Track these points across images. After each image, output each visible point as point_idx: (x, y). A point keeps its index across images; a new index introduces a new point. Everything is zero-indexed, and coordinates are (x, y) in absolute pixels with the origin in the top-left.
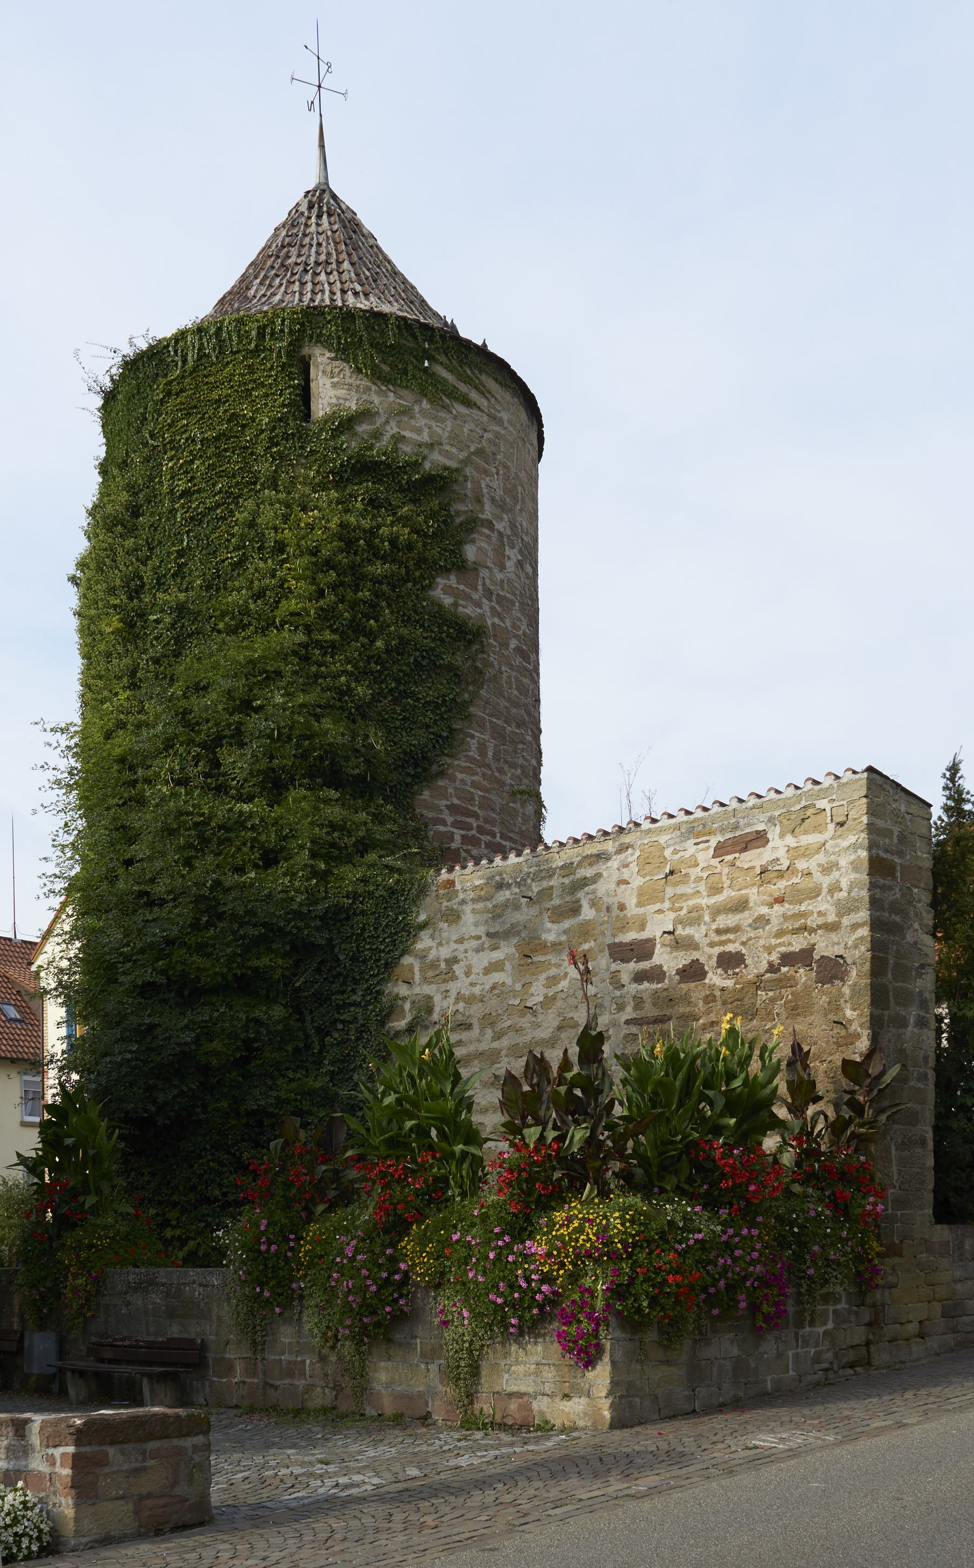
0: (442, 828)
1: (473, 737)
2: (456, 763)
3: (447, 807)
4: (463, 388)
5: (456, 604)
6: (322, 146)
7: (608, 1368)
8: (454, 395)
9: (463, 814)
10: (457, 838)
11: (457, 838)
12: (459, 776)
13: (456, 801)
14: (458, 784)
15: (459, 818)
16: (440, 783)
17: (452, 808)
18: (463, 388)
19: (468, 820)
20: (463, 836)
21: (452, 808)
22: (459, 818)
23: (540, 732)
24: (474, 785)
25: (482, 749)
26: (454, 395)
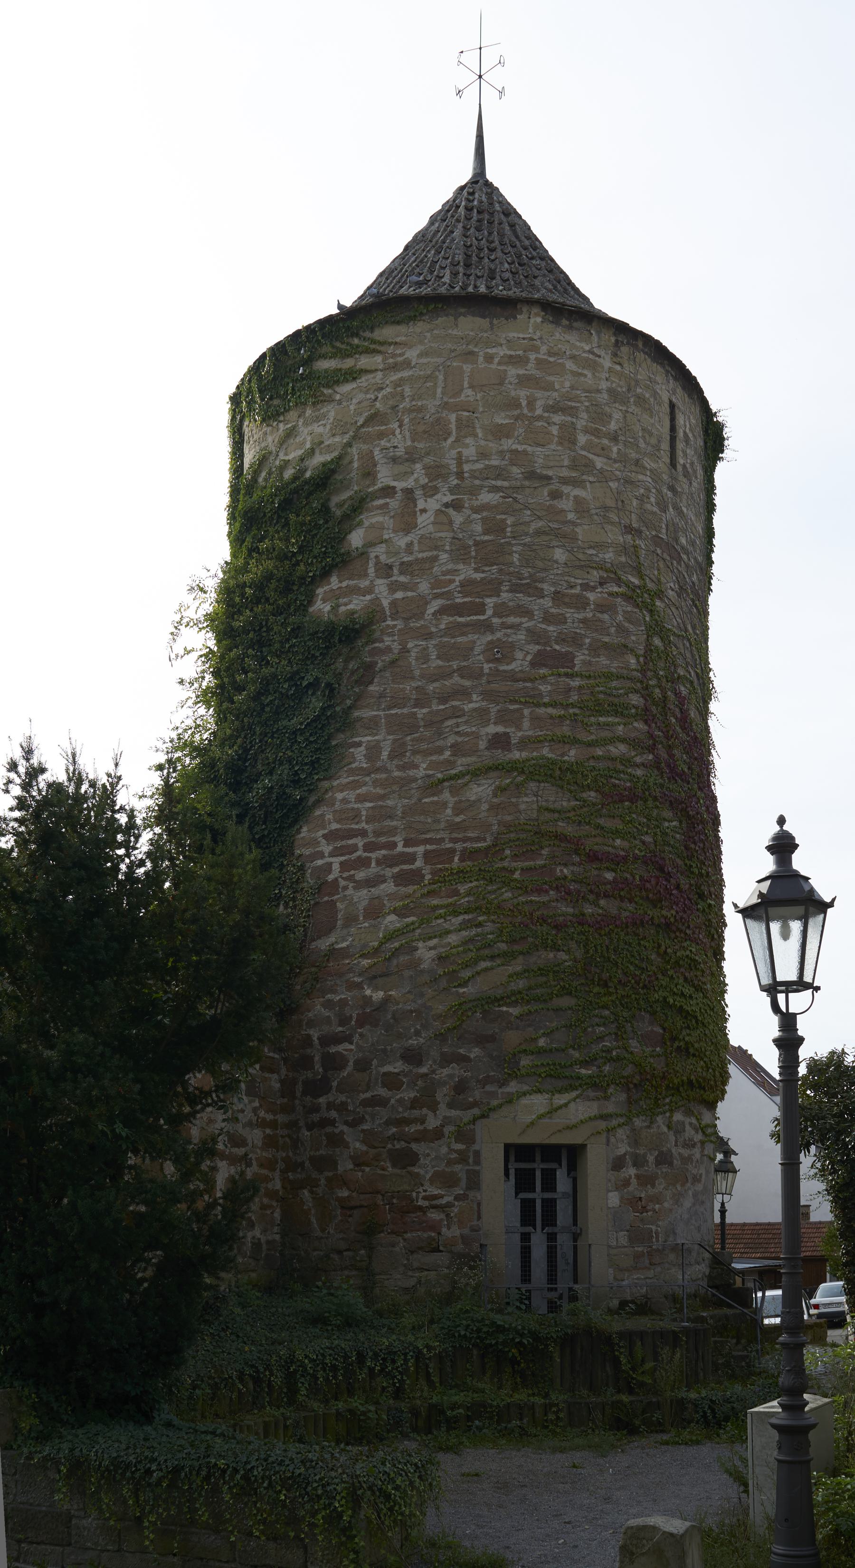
0: (320, 862)
1: (359, 744)
2: (335, 783)
3: (325, 836)
4: (348, 363)
5: (335, 608)
6: (815, 970)
7: (319, 941)
8: (673, 524)
9: (344, 838)
10: (336, 867)
11: (336, 867)
12: (339, 796)
13: (335, 826)
14: (338, 806)
15: (339, 844)
16: (318, 813)
17: (330, 837)
18: (348, 363)
19: (350, 842)
20: (341, 863)
21: (330, 837)
22: (339, 844)
23: (719, 824)
24: (361, 799)
25: (373, 752)
26: (673, 524)
